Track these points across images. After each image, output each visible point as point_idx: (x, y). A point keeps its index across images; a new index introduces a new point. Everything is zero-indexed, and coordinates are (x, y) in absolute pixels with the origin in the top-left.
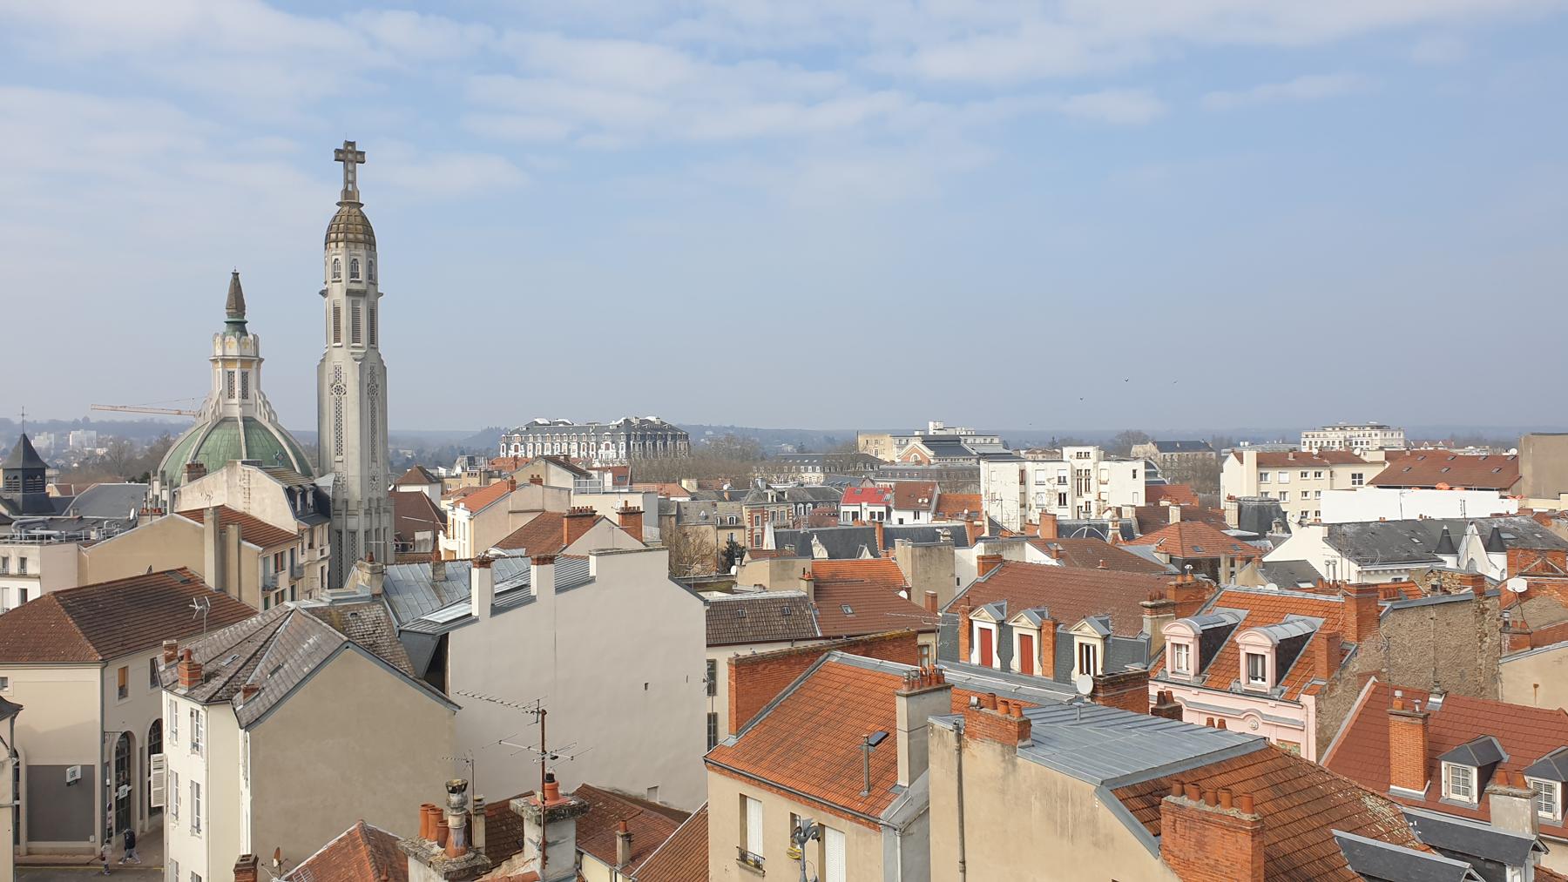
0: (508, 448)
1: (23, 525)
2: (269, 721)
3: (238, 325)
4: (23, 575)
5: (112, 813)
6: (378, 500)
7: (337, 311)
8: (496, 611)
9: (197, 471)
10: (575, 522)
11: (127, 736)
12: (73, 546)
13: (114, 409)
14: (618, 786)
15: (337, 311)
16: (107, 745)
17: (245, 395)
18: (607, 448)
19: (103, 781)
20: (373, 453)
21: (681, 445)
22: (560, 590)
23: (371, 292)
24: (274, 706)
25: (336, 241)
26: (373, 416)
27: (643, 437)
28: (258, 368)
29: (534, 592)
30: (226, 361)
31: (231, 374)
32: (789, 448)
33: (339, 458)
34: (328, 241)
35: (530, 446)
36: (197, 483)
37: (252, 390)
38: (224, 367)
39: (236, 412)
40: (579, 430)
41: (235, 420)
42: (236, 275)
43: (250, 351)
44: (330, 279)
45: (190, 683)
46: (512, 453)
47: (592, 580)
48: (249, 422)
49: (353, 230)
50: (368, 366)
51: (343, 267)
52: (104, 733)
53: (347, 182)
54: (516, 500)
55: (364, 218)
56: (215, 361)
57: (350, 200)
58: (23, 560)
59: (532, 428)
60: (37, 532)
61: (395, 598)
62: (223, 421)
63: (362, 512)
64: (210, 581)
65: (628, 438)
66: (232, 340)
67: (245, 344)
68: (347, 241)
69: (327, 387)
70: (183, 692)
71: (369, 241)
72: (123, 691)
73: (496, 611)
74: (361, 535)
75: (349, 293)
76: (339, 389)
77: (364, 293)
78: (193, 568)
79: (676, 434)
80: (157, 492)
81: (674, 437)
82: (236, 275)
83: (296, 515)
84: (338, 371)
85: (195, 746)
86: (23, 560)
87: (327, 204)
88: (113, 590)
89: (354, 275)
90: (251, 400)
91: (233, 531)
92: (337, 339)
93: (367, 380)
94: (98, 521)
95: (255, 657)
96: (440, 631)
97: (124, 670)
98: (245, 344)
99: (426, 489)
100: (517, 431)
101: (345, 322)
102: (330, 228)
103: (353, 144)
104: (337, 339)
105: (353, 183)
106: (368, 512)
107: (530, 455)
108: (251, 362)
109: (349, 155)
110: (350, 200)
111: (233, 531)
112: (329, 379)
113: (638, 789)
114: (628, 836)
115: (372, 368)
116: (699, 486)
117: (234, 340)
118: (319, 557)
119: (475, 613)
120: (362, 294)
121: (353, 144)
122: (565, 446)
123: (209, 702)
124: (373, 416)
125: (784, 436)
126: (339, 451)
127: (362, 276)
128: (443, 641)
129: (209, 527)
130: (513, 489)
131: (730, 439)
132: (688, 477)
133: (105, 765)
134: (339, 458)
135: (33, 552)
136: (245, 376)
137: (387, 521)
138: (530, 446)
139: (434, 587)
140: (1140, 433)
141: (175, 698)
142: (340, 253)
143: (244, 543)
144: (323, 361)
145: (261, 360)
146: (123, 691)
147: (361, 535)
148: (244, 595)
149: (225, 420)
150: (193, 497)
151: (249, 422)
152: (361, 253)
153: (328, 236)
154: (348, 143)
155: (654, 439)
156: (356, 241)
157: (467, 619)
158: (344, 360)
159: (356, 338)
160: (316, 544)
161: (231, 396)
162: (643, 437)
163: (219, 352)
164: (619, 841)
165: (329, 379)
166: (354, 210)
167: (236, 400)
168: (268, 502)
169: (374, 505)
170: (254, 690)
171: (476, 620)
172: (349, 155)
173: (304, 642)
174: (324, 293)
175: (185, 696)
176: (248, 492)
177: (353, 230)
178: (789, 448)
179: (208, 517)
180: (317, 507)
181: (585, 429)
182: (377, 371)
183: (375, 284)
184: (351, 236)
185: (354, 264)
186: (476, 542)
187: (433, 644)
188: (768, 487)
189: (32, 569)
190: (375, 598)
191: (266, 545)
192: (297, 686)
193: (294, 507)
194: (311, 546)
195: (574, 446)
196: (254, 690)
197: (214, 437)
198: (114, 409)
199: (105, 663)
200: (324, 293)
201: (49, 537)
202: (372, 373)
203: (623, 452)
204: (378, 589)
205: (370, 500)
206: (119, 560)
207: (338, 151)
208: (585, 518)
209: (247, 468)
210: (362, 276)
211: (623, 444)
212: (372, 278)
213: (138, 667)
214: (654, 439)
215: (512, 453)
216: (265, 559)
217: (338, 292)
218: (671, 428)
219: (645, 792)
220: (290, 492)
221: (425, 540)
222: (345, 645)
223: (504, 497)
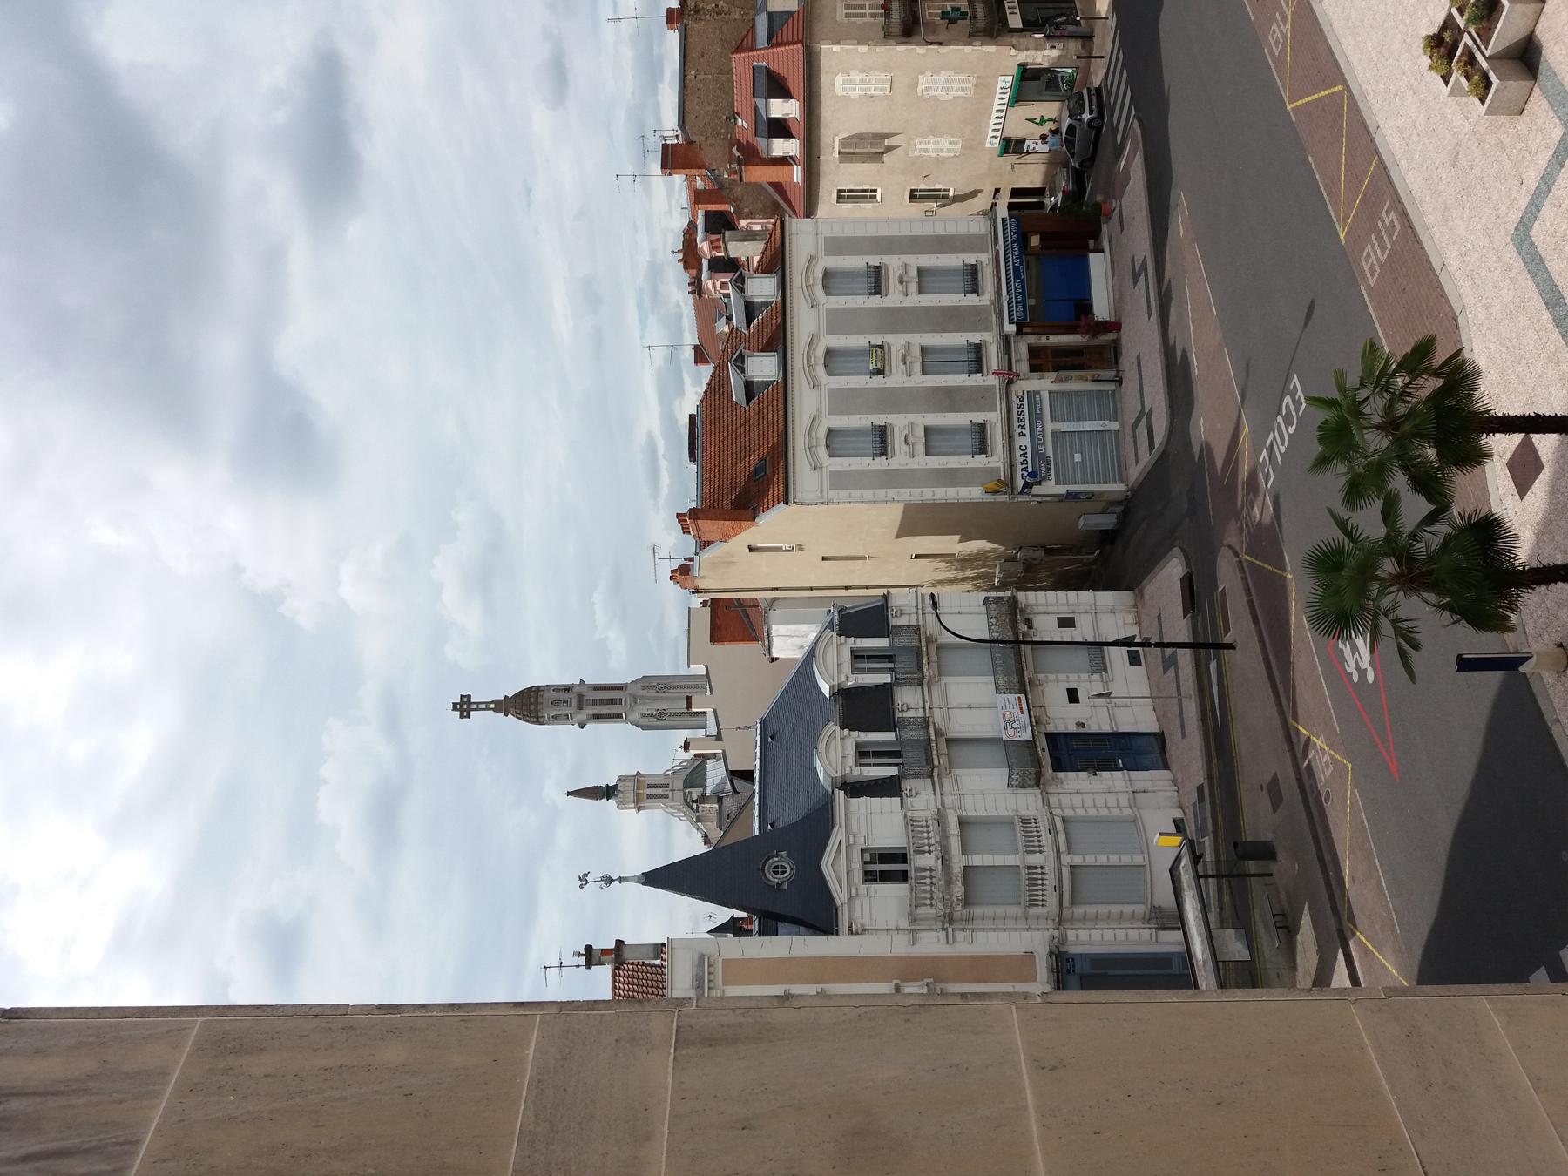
3: (609, 792)
13: (846, 588)
31: (649, 796)
42: (569, 794)
49: (528, 705)
53: (487, 709)
57: (503, 706)
82: (569, 794)
84: (643, 715)
101: (605, 710)
109: (464, 707)
110: (503, 706)
120: (580, 697)
121: (462, 716)
136: (650, 786)
140: (685, 233)
142: (548, 713)
145: (620, 943)
154: (455, 708)
156: (536, 703)
159: (618, 702)
177: (528, 705)
207: (462, 716)
210: (566, 696)
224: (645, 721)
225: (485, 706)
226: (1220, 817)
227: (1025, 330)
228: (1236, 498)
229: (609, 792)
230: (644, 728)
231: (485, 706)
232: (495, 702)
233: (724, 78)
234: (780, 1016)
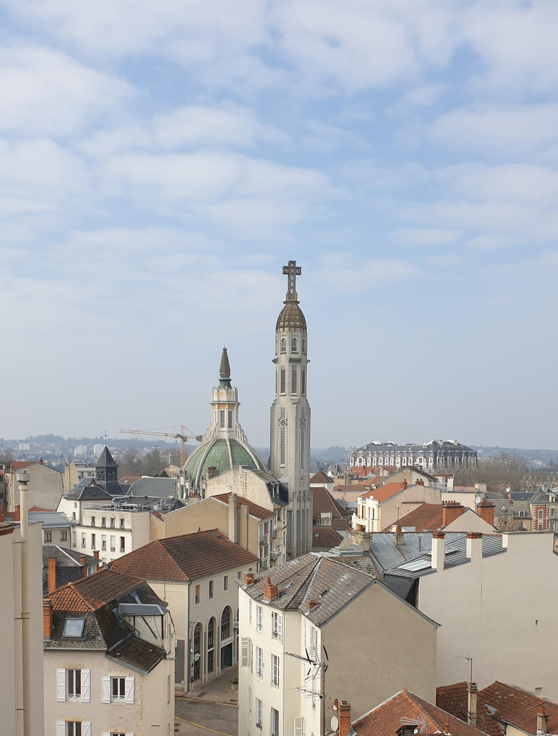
0: (355, 461)
1: (116, 500)
2: (331, 623)
3: (226, 382)
4: (122, 529)
5: (192, 669)
6: (304, 492)
7: (283, 372)
8: (447, 566)
9: (214, 472)
10: (451, 511)
11: (199, 624)
12: (147, 513)
13: (132, 432)
14: (518, 685)
15: (283, 372)
16: (190, 629)
17: (230, 426)
18: (421, 460)
19: (189, 650)
20: (302, 462)
21: (472, 460)
22: (485, 555)
23: (303, 360)
24: (334, 615)
25: (284, 327)
26: (303, 439)
27: (445, 454)
28: (237, 409)
29: (469, 556)
30: (220, 404)
31: (222, 412)
32: (540, 463)
33: (282, 465)
34: (278, 327)
35: (369, 459)
36: (216, 479)
37: (234, 423)
38: (219, 408)
39: (225, 436)
40: (401, 448)
41: (225, 441)
42: (225, 350)
43: (233, 399)
44: (279, 352)
45: (272, 597)
46: (363, 463)
47: (505, 550)
48: (232, 441)
49: (292, 319)
50: (300, 407)
51: (287, 343)
52: (189, 622)
53: (290, 287)
54: (407, 495)
55: (300, 311)
56: (213, 404)
57: (292, 299)
58: (122, 521)
59: (371, 447)
60: (125, 504)
61: (377, 554)
62: (218, 441)
63: (296, 499)
64: (232, 538)
65: (435, 454)
66: (223, 391)
67: (230, 394)
68: (290, 326)
69: (276, 420)
70: (267, 602)
71: (304, 328)
72: (197, 600)
73: (447, 566)
74: (295, 513)
75: (291, 360)
76: (283, 423)
77: (299, 361)
78: (221, 529)
79: (469, 452)
80: (182, 483)
81: (466, 454)
82: (225, 350)
83: (273, 500)
84: (283, 410)
85: (275, 634)
86: (122, 521)
87: (278, 305)
88: (186, 539)
89: (294, 349)
90: (233, 429)
91: (244, 509)
92: (283, 391)
93: (300, 417)
94: (156, 499)
95: (305, 585)
96: (414, 576)
97: (198, 587)
98: (230, 394)
99: (325, 486)
100: (361, 449)
102: (279, 318)
103: (294, 262)
104: (283, 391)
105: (294, 288)
106: (299, 500)
107: (398, 466)
108: (233, 405)
109: (292, 270)
110: (292, 299)
111: (244, 509)
112: (277, 416)
113: (529, 688)
114: (546, 717)
115: (303, 408)
116: (488, 489)
117: (224, 391)
118: (283, 526)
119: (434, 566)
120: (298, 361)
121: (294, 262)
122: (392, 459)
123: (286, 609)
124: (303, 439)
125: (537, 454)
126: (283, 462)
127: (299, 350)
128: (417, 581)
129: (231, 505)
130: (405, 488)
131: (504, 455)
132: (479, 482)
133: (190, 641)
134: (282, 465)
135: (128, 516)
136: (230, 413)
137: (309, 505)
138: (369, 459)
139: (398, 549)
141: (260, 605)
142: (286, 335)
143: (250, 516)
144: (274, 404)
145: (239, 404)
146: (197, 600)
147: (295, 513)
148: (250, 546)
149: (219, 441)
150: (215, 488)
151: (232, 441)
152: (298, 334)
153: (278, 323)
155: (453, 455)
156: (295, 327)
157: (429, 570)
158: (286, 402)
159: (294, 390)
160: (282, 519)
161: (222, 426)
162: (445, 454)
163: (216, 399)
164: (540, 720)
165: (277, 416)
166: (294, 306)
167: (225, 429)
168: (258, 493)
169: (302, 495)
170: (315, 604)
171: (435, 571)
172: (292, 270)
173: (340, 578)
174: (275, 361)
175: (270, 605)
176: (245, 485)
177: (292, 319)
178: (540, 463)
179: (231, 499)
180: (280, 494)
181: (406, 448)
182: (305, 411)
183: (306, 355)
184: (292, 323)
185: (294, 341)
186: (382, 520)
187: (410, 584)
188: (549, 491)
189: (127, 526)
190: (366, 553)
191: (263, 518)
192: (347, 604)
193: (271, 494)
194: (279, 519)
195: (398, 460)
196: (315, 604)
197: (213, 451)
198: (132, 432)
199: (190, 582)
200: (275, 361)
201: (132, 508)
202: (302, 412)
203: (431, 464)
204: (367, 549)
205: (300, 492)
206: (185, 524)
207: (285, 268)
208: (456, 509)
209: (245, 470)
210: (299, 350)
211: (431, 459)
212: (304, 351)
213: (204, 584)
214: (453, 455)
215: (357, 463)
216: (261, 526)
217: (284, 360)
218: (465, 448)
219: (534, 690)
220: (269, 486)
221: (327, 518)
222: (374, 581)
223: (398, 493)
224: (278, 409)
225: (292, 286)
226: (5, 529)
227: (49, 539)
228: (467, 708)
229: (226, 382)
230: (273, 409)
231: (292, 286)
232: (295, 294)
233: (156, 508)
234: (122, 704)
